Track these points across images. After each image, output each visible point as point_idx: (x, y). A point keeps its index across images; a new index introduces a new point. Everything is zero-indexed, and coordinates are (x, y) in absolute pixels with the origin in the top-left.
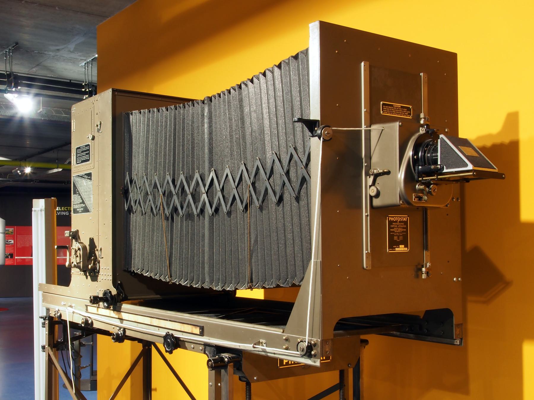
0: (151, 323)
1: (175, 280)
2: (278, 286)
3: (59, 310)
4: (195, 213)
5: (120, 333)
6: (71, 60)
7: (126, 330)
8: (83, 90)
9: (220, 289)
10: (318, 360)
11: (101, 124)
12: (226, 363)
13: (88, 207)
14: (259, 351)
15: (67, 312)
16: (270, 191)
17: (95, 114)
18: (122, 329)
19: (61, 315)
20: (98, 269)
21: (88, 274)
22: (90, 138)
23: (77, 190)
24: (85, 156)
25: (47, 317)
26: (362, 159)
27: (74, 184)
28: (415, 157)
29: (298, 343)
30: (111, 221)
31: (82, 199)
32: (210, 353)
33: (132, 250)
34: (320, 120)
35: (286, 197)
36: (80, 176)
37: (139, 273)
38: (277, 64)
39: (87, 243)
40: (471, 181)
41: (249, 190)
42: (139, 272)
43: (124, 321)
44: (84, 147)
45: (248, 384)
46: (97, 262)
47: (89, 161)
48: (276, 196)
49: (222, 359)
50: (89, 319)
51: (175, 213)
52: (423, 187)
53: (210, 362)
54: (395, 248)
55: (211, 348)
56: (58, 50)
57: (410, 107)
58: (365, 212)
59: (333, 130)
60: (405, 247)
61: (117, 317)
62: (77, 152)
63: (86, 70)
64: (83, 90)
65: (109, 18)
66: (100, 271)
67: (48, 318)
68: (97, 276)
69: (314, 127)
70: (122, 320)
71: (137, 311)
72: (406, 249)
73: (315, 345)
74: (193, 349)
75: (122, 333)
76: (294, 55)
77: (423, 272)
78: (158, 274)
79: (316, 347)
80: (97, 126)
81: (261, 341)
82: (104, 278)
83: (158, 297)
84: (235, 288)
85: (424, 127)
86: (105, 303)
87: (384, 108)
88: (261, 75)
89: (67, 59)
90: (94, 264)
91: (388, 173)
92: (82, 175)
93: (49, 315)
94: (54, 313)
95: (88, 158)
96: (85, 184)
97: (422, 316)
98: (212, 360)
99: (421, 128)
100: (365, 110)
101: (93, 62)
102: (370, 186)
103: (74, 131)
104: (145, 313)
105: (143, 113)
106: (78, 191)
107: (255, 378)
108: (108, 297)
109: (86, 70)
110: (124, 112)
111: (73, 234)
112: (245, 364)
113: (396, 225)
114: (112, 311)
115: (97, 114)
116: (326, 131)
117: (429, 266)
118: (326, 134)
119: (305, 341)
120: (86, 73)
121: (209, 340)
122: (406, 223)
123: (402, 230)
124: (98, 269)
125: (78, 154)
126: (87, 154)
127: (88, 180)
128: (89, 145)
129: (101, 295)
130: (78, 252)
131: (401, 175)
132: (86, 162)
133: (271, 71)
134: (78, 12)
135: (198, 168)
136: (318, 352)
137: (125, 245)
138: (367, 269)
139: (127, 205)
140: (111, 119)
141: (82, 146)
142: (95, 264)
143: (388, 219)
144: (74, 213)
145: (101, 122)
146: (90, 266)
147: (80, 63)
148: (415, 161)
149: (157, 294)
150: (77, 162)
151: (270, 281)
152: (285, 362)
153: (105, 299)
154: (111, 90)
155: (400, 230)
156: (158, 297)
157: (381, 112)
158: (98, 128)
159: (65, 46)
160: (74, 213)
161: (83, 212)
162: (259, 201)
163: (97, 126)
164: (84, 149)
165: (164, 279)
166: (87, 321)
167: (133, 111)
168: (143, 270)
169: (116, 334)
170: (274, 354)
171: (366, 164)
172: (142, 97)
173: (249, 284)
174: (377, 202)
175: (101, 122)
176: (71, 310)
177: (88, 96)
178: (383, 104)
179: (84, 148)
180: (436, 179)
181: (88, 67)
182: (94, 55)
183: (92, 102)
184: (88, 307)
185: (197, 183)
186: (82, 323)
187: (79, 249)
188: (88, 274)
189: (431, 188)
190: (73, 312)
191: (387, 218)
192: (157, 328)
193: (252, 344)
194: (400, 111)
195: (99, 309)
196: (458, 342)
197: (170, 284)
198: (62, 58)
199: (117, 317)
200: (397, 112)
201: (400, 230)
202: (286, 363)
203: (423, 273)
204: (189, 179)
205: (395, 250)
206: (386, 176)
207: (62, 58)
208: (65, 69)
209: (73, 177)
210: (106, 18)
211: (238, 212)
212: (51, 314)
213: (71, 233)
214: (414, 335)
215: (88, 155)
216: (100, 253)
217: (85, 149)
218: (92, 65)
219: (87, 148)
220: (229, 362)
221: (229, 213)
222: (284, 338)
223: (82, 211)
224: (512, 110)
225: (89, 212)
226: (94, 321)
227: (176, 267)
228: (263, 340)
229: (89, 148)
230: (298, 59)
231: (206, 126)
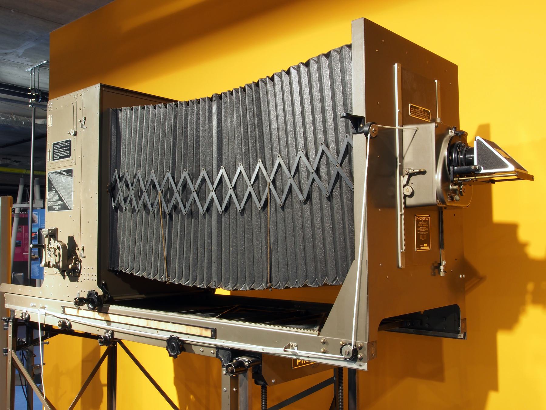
0: (147, 325)
1: (173, 280)
2: (305, 286)
3: (27, 312)
4: (201, 211)
5: (107, 335)
6: (17, 65)
7: (114, 332)
8: (30, 94)
9: (205, 287)
10: (365, 364)
11: (85, 119)
12: (246, 367)
13: (67, 204)
14: (288, 355)
15: (39, 314)
16: (296, 188)
17: (78, 109)
18: (110, 332)
19: (29, 317)
20: (79, 269)
21: (66, 274)
22: (72, 134)
23: (52, 187)
24: (64, 152)
25: (11, 319)
26: (396, 159)
27: (49, 181)
28: (450, 158)
29: (340, 347)
30: (97, 219)
31: (59, 196)
32: (224, 357)
33: (120, 249)
34: (365, 116)
35: (315, 195)
36: (57, 172)
37: (128, 273)
38: (304, 62)
39: (66, 242)
40: (496, 183)
41: (269, 188)
42: (128, 271)
43: (112, 323)
44: (62, 143)
45: (264, 388)
46: (79, 261)
47: (70, 157)
48: (303, 194)
49: (241, 363)
50: (66, 321)
51: (174, 211)
52: (457, 187)
53: (230, 368)
54: (421, 247)
55: (225, 351)
56: (5, 54)
57: (429, 111)
58: (400, 211)
59: (379, 127)
60: (428, 246)
61: (103, 318)
62: (53, 148)
63: (33, 76)
64: (30, 94)
65: (64, 26)
66: (82, 271)
67: (12, 320)
68: (78, 276)
69: (358, 123)
70: (109, 322)
71: (130, 313)
72: (428, 247)
73: (361, 348)
74: (213, 355)
75: (110, 336)
76: (326, 52)
77: (441, 270)
78: (151, 274)
79: (362, 350)
80: (81, 121)
81: (291, 344)
82: (94, 279)
83: (143, 296)
84: (249, 288)
85: (453, 130)
86: (89, 304)
87: (412, 110)
88: (283, 73)
89: (14, 63)
90: (75, 264)
91: (424, 173)
92: (60, 172)
93: (14, 316)
94: (21, 315)
95: (69, 154)
96: (64, 181)
97: (422, 313)
98: (233, 365)
99: (450, 131)
100: (399, 110)
101: (40, 68)
102: (404, 186)
103: (50, 127)
104: (141, 314)
105: (136, 109)
106: (54, 188)
107: (273, 381)
108: (93, 298)
109: (33, 76)
110: (111, 109)
111: (52, 232)
112: (265, 370)
113: (421, 224)
114: (97, 313)
115: (81, 110)
116: (373, 129)
117: (445, 264)
118: (374, 131)
119: (350, 344)
120: (33, 79)
121: (223, 342)
122: (428, 222)
123: (426, 229)
124: (79, 269)
125: (55, 150)
126: (66, 150)
127: (68, 176)
128: (70, 141)
129: (85, 297)
130: (56, 251)
131: (438, 176)
132: (65, 158)
133: (296, 69)
134: (34, 16)
135: (205, 166)
136: (364, 355)
137: (110, 244)
138: (402, 268)
139: (114, 203)
140: (98, 115)
141: (61, 141)
142: (75, 264)
143: (416, 217)
144: (49, 210)
145: (85, 117)
146: (70, 266)
147: (26, 68)
148: (450, 162)
149: (141, 294)
150: (54, 159)
151: (295, 280)
152: (298, 361)
153: (90, 300)
154: (99, 85)
155: (424, 229)
156: (143, 296)
157: (410, 114)
158: (82, 124)
159: (14, 50)
160: (49, 210)
161: (60, 209)
162: (262, 199)
163: (81, 121)
164: (63, 145)
165: (160, 279)
166: (64, 323)
167: (123, 108)
168: (133, 269)
169: (103, 337)
170: (308, 357)
171: (400, 164)
172: (128, 94)
173: (268, 284)
174: (410, 202)
175: (85, 117)
176: (44, 312)
177: (35, 100)
178: (411, 106)
179: (64, 144)
180: (474, 179)
181: (34, 73)
182: (42, 62)
183: (74, 97)
184: (66, 308)
185: (204, 180)
186: (59, 325)
187: (59, 248)
188: (66, 274)
189: (462, 188)
190: (46, 314)
191: (415, 217)
192: (156, 331)
193: (283, 348)
194: (422, 114)
195: (79, 310)
196: (462, 336)
197: (168, 284)
198: (8, 62)
199: (104, 319)
200: (420, 115)
201: (424, 229)
202: (299, 363)
203: (441, 271)
204: (194, 176)
205: (421, 249)
206: (421, 175)
207: (8, 62)
208: (9, 73)
209: (49, 173)
210: (62, 25)
211: (253, 210)
212: (16, 315)
213: (50, 232)
214: (414, 330)
215: (69, 151)
216: (82, 252)
217: (64, 145)
218: (39, 71)
219: (68, 144)
220: (249, 366)
221: (243, 212)
222: (322, 340)
223: (59, 208)
224: (484, 122)
225: (69, 210)
226: (72, 324)
227: (176, 267)
228: (293, 342)
229: (70, 143)
230: (330, 58)
231: (214, 123)
